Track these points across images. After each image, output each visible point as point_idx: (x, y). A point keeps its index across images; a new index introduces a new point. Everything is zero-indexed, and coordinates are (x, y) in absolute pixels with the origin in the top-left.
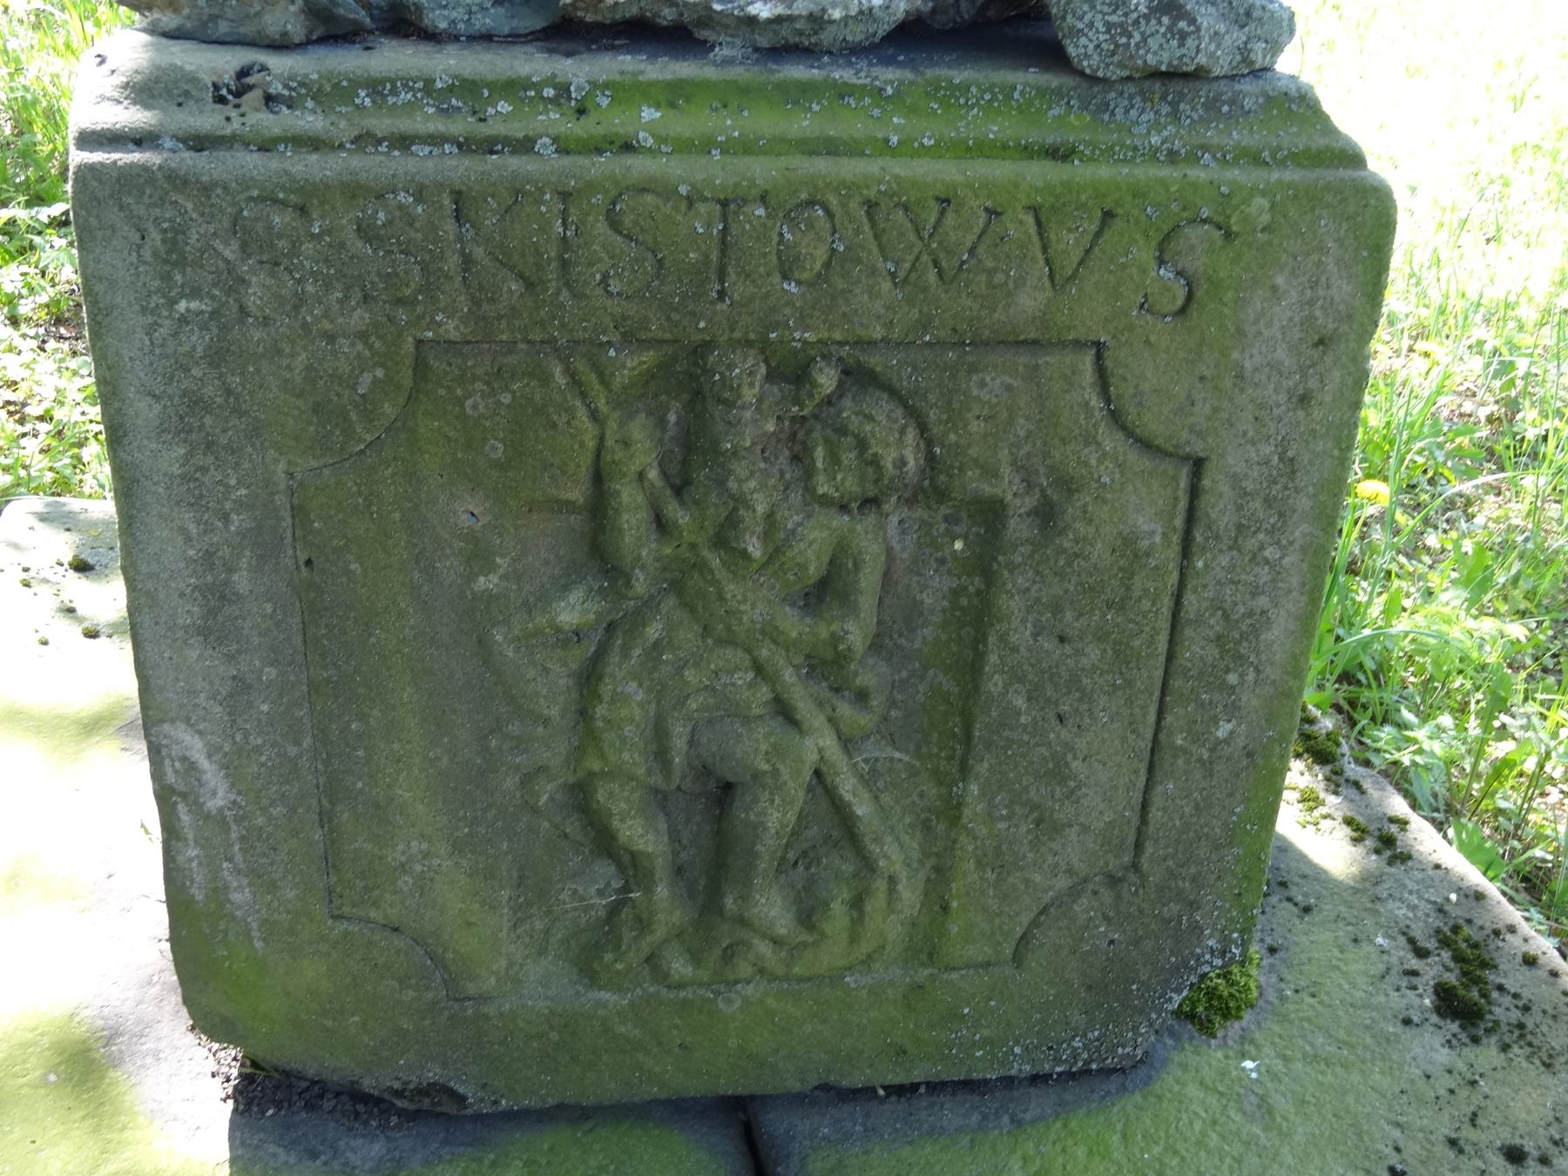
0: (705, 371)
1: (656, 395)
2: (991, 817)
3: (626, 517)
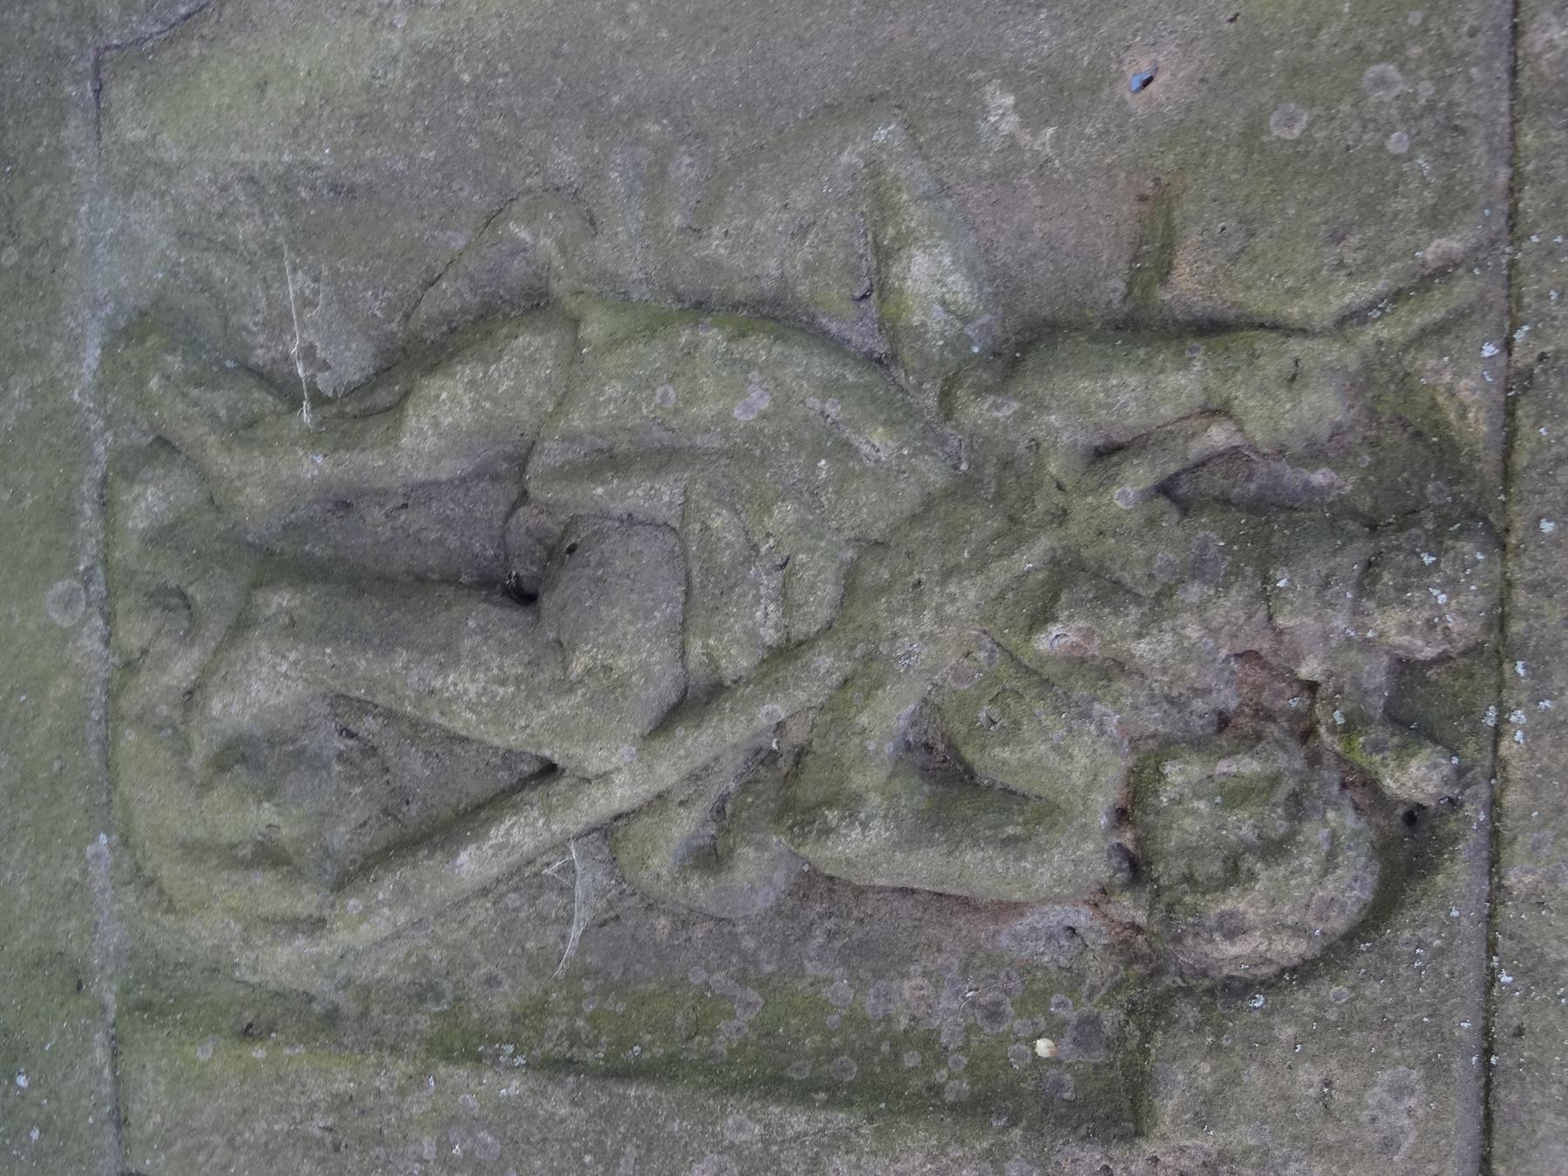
0: (1438, 535)
1: (1374, 444)
2: (448, 1123)
3: (1133, 381)
